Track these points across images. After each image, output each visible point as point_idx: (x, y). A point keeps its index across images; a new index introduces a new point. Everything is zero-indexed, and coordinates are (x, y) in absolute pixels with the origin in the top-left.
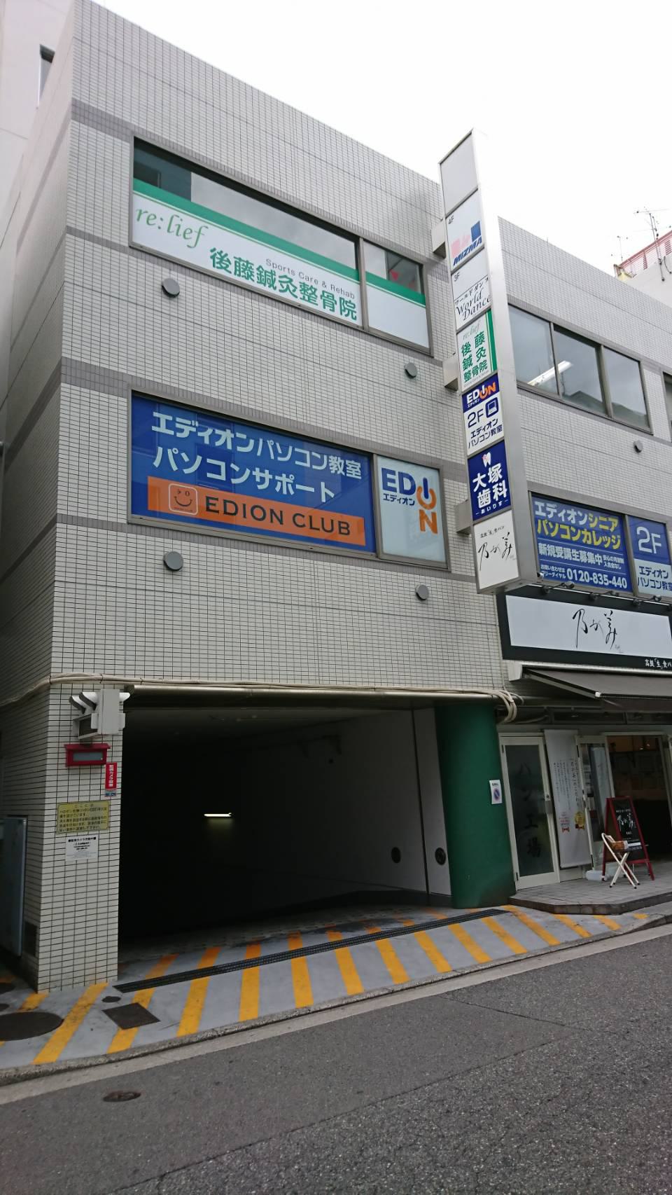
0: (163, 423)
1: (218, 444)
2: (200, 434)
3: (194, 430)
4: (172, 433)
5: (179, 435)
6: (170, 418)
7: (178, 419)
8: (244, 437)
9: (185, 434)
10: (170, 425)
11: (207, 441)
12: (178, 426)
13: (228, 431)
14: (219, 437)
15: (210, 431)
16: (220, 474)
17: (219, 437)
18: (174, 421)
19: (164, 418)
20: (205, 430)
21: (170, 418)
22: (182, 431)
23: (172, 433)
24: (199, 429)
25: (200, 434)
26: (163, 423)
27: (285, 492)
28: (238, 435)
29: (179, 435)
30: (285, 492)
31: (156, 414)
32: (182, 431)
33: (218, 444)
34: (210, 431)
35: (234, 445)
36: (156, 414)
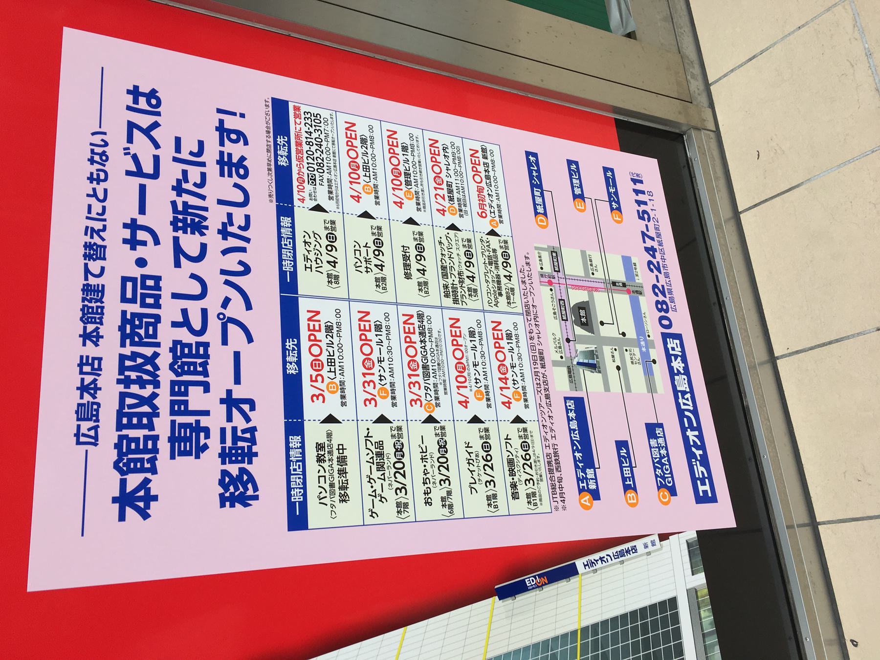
4: (707, 480)
9: (702, 469)
19: (701, 488)
22: (702, 472)
23: (707, 480)
24: (697, 459)
29: (706, 475)
31: (701, 494)
32: (702, 472)
36: (701, 494)
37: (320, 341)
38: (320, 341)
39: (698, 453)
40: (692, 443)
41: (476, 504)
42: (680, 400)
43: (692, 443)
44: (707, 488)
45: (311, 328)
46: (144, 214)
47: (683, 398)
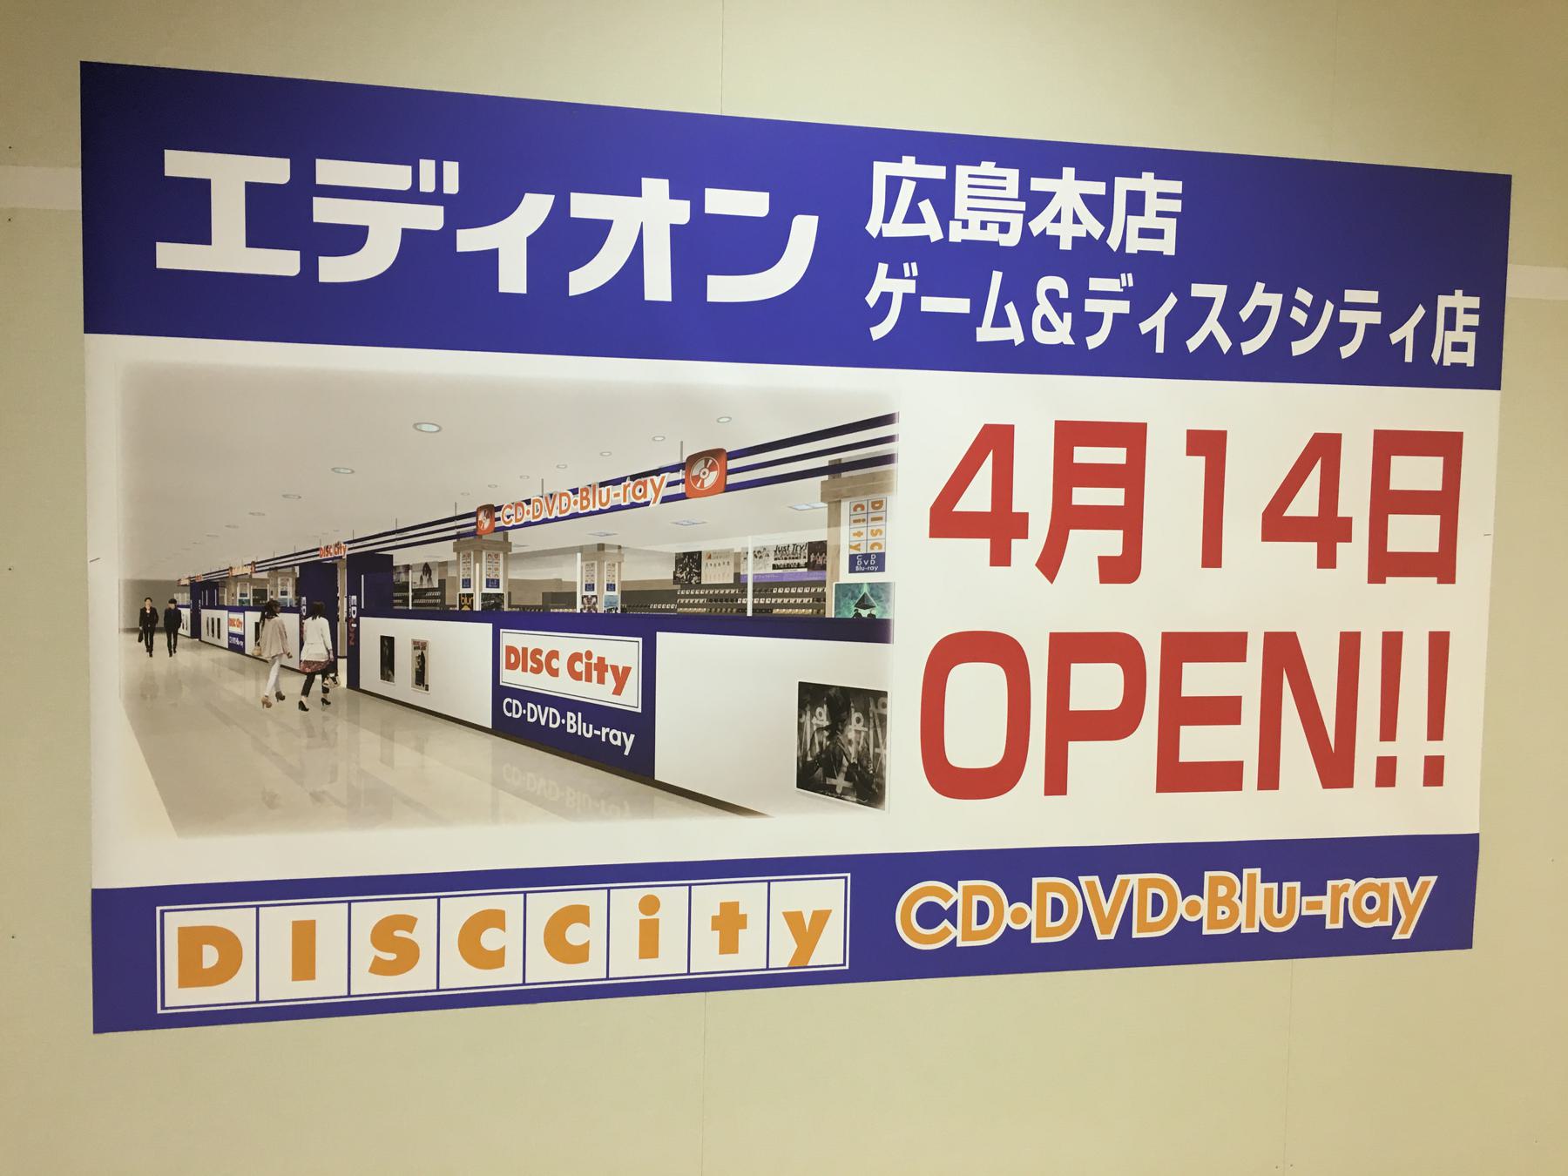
0: (229, 214)
1: (584, 280)
2: (469, 240)
3: (431, 218)
4: (284, 263)
5: (333, 270)
6: (277, 171)
7: (329, 171)
8: (753, 204)
9: (375, 259)
10: (274, 216)
11: (513, 278)
12: (326, 211)
13: (655, 188)
14: (599, 231)
15: (535, 209)
16: (1211, 336)
17: (599, 231)
18: (304, 186)
19: (230, 177)
20: (500, 209)
21: (277, 171)
22: (351, 239)
23: (284, 263)
24: (463, 211)
25: (469, 240)
26: (229, 214)
27: (1176, 206)
28: (720, 201)
29: (333, 270)
30: (1176, 206)
31: (180, 164)
32: (351, 239)
33: (584, 280)
34: (535, 209)
35: (688, 273)
36: (180, 164)
37: (1056, 783)
38: (1056, 783)
39: (508, 241)
40: (584, 206)
41: (1393, 890)
42: (908, 167)
43: (584, 206)
44: (228, 250)
45: (1200, 679)
46: (1219, 565)
47: (924, 188)
